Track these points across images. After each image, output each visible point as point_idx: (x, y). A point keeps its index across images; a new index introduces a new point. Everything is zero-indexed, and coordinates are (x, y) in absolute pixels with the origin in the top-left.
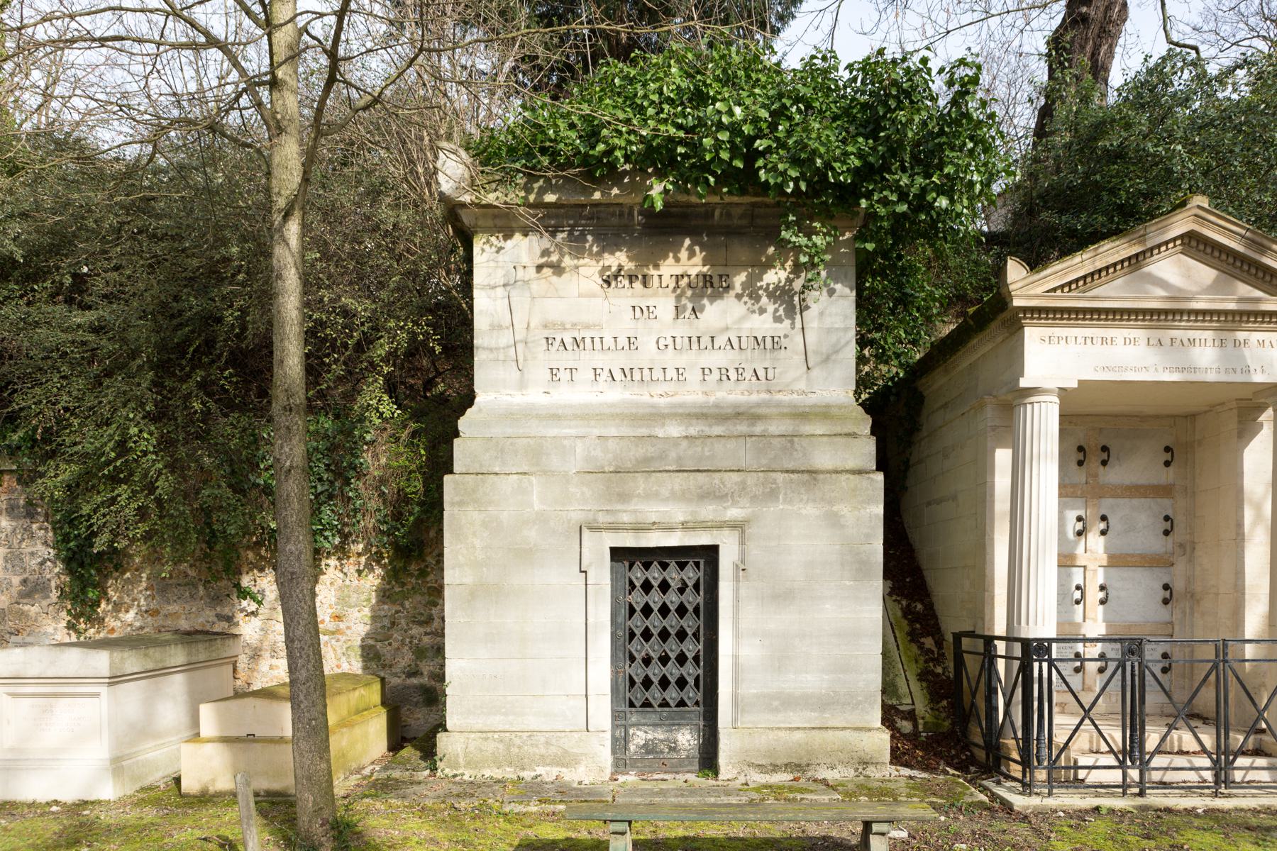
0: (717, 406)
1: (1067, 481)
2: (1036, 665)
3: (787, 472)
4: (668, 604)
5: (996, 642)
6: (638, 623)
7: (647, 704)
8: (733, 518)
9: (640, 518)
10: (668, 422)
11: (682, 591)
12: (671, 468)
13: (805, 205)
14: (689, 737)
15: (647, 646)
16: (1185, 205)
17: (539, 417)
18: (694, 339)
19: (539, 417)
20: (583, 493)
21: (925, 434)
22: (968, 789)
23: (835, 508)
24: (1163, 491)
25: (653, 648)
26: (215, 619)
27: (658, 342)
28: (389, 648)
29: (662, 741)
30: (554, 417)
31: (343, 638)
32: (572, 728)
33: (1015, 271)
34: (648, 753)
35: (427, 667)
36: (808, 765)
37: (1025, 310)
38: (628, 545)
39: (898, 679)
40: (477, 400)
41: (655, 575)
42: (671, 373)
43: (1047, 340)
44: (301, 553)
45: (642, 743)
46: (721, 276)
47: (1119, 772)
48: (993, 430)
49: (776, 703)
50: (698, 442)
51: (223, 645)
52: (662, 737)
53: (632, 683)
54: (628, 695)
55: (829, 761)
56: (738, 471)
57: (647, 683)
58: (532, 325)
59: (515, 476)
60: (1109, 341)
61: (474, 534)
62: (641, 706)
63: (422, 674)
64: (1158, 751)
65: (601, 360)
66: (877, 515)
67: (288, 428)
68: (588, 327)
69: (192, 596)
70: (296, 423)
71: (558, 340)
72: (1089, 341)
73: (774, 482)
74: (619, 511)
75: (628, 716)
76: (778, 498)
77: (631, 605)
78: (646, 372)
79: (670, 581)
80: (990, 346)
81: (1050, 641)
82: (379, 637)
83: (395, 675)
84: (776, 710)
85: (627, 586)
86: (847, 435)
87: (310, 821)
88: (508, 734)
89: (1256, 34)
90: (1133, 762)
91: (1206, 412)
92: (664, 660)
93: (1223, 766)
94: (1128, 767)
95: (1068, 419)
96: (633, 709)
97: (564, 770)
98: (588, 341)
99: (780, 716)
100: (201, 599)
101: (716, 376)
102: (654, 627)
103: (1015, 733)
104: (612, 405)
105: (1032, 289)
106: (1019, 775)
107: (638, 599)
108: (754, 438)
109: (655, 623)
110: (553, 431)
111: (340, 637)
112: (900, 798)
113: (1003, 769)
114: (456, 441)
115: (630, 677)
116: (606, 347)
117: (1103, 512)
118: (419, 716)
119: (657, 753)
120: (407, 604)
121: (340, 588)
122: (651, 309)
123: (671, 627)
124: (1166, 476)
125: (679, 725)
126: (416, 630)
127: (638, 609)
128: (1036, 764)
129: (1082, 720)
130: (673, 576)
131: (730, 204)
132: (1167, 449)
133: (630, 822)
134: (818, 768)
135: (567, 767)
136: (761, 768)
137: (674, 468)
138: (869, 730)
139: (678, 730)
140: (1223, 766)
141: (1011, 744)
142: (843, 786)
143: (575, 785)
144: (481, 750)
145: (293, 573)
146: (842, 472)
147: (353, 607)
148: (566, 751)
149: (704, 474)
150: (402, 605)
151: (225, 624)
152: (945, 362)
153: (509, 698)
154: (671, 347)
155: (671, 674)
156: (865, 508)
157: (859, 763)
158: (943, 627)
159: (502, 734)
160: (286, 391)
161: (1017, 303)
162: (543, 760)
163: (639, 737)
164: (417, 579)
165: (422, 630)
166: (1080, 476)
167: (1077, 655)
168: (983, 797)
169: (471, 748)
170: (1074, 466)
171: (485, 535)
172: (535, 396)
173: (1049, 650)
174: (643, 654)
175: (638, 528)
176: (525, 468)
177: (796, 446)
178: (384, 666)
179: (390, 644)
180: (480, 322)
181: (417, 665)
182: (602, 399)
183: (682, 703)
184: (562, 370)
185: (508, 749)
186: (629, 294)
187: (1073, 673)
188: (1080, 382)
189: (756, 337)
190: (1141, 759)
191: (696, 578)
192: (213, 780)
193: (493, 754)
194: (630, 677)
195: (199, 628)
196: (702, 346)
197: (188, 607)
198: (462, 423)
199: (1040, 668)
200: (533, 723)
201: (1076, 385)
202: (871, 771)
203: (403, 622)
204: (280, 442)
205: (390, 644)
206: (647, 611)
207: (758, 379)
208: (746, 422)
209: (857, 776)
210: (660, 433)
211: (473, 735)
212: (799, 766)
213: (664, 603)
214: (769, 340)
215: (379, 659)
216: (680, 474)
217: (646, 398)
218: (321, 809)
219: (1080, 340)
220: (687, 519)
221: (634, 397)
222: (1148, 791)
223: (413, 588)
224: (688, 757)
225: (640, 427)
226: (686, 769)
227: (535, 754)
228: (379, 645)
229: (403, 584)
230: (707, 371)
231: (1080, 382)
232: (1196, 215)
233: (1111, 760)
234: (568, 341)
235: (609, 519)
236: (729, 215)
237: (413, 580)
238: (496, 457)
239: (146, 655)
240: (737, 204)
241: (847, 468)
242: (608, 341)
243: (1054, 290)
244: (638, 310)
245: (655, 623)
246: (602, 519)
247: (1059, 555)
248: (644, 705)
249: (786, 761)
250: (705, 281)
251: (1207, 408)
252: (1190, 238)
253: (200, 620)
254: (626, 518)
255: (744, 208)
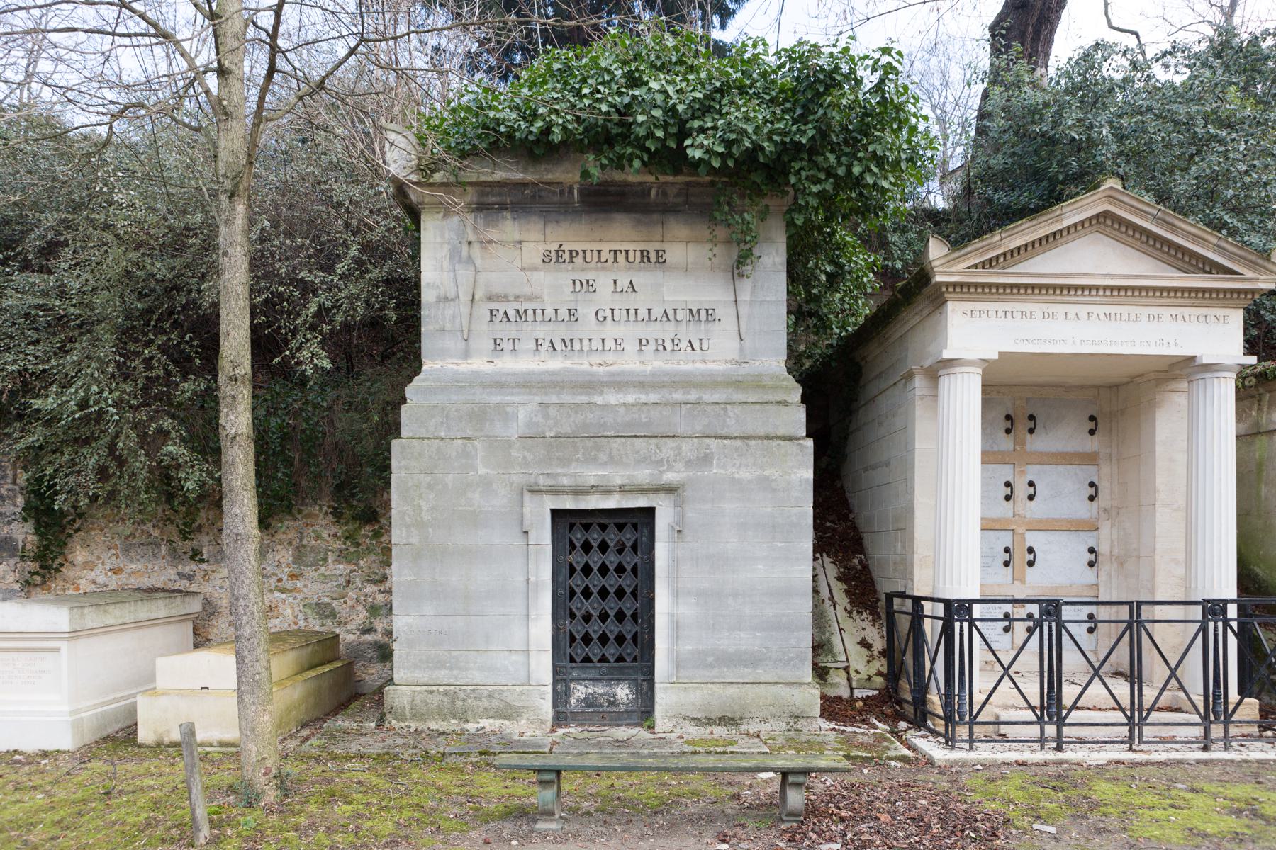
0: (654, 374)
1: (988, 448)
2: (957, 625)
3: (721, 437)
4: (608, 563)
5: (923, 602)
6: (578, 582)
7: (587, 659)
8: (669, 482)
9: (580, 481)
10: (606, 390)
11: (620, 551)
12: (609, 434)
13: (736, 184)
14: (627, 691)
15: (587, 604)
16: (1099, 187)
17: (484, 386)
18: (632, 312)
19: (484, 386)
20: (524, 458)
21: (862, 403)
22: (893, 743)
23: (767, 473)
24: (1089, 459)
25: (593, 606)
26: (177, 578)
27: (597, 314)
28: (344, 605)
29: (601, 695)
30: (498, 384)
31: (300, 596)
32: (514, 682)
33: (936, 250)
34: (588, 706)
35: (380, 625)
36: (741, 719)
37: (947, 285)
38: (568, 507)
39: (833, 638)
40: (424, 368)
41: (595, 537)
42: (610, 344)
43: (969, 313)
44: (245, 515)
45: (582, 697)
46: (657, 252)
47: (1037, 727)
48: (922, 399)
49: (710, 659)
50: (635, 409)
51: (183, 602)
52: (601, 691)
53: (573, 639)
54: (569, 650)
55: (761, 715)
56: (674, 436)
57: (587, 639)
58: (477, 297)
59: (460, 441)
60: (1028, 315)
61: (420, 496)
62: (581, 662)
63: (376, 631)
64: (1074, 707)
65: (542, 331)
66: (807, 480)
67: (233, 397)
68: (530, 298)
69: (154, 555)
70: (242, 392)
71: (502, 312)
72: (1009, 315)
73: (708, 447)
74: (559, 475)
75: (569, 671)
76: (711, 463)
77: (571, 564)
78: (586, 342)
79: (609, 542)
80: (918, 318)
81: (972, 601)
82: (335, 596)
83: (350, 632)
84: (711, 666)
85: (568, 546)
86: (779, 403)
87: (253, 771)
88: (452, 688)
89: (1201, 19)
90: (1050, 717)
91: (1128, 383)
92: (604, 617)
93: (1136, 721)
94: (1046, 723)
95: (991, 391)
96: (574, 665)
97: (506, 722)
98: (530, 312)
99: (715, 672)
100: (163, 558)
101: (652, 346)
102: (594, 586)
103: (939, 689)
104: (553, 373)
105: (953, 265)
106: (942, 730)
107: (578, 559)
108: (689, 406)
109: (596, 581)
110: (496, 399)
111: (297, 595)
112: (826, 752)
113: (929, 723)
114: (404, 408)
115: (571, 634)
116: (547, 318)
117: (1029, 478)
118: (373, 671)
119: (597, 706)
120: (362, 563)
121: (298, 548)
122: (591, 282)
123: (610, 585)
124: (1090, 444)
125: (618, 680)
126: (371, 589)
127: (578, 568)
128: (957, 719)
129: (1002, 678)
130: (612, 537)
131: (666, 183)
132: (1092, 418)
133: (558, 772)
134: (750, 721)
135: (509, 719)
136: (697, 721)
137: (612, 433)
138: (800, 684)
139: (618, 685)
140: (1136, 721)
141: (935, 700)
142: (774, 739)
143: (516, 737)
144: (427, 703)
145: (237, 535)
146: (773, 438)
147: (310, 566)
148: (508, 704)
149: (641, 439)
150: (357, 564)
151: (185, 583)
152: (878, 334)
153: (454, 654)
154: (609, 319)
155: (611, 631)
156: (795, 473)
157: (791, 717)
158: (878, 588)
159: (447, 688)
160: (232, 362)
161: (938, 278)
162: (487, 713)
163: (580, 691)
164: (371, 539)
165: (376, 588)
166: (1006, 443)
167: (1007, 616)
168: (906, 752)
169: (418, 701)
170: (1002, 434)
171: (431, 497)
172: (479, 364)
173: (969, 611)
174: (583, 611)
175: (578, 492)
176: (470, 434)
177: (730, 413)
178: (339, 624)
179: (345, 602)
180: (428, 296)
181: (371, 623)
182: (543, 367)
183: (620, 659)
184: (505, 340)
185: (453, 702)
186: (570, 268)
187: (1002, 632)
188: (1000, 353)
189: (691, 310)
190: (1059, 713)
191: (634, 539)
192: (168, 731)
193: (438, 706)
194: (571, 634)
195: (160, 586)
196: (640, 318)
197: (150, 566)
198: (410, 391)
199: (961, 627)
200: (476, 676)
201: (996, 357)
202: (802, 724)
203: (357, 580)
204: (225, 410)
205: (345, 602)
206: (587, 570)
207: (693, 349)
208: (681, 391)
209: (789, 730)
210: (599, 400)
211: (418, 688)
212: (732, 719)
213: (603, 563)
214: (703, 313)
215: (335, 617)
216: (618, 439)
217: (586, 367)
218: (264, 759)
219: (1001, 314)
220: (624, 482)
221: (575, 366)
222: (1064, 746)
223: (367, 548)
224: (626, 711)
225: (581, 394)
226: (625, 722)
227: (478, 707)
228: (335, 603)
229: (358, 545)
230: (644, 342)
231: (1000, 353)
232: (1109, 196)
233: (1029, 715)
234: (512, 313)
235: (550, 482)
236: (665, 194)
237: (368, 541)
238: (442, 423)
239: (105, 611)
240: (673, 184)
241: (779, 434)
242: (550, 312)
243: (976, 266)
244: (578, 283)
245: (596, 581)
246: (543, 482)
247: (982, 519)
248: (601, 660)
249: (720, 715)
250: (642, 257)
251: (1128, 380)
252: (1105, 218)
253: (162, 578)
254: (565, 481)
255: (678, 186)
